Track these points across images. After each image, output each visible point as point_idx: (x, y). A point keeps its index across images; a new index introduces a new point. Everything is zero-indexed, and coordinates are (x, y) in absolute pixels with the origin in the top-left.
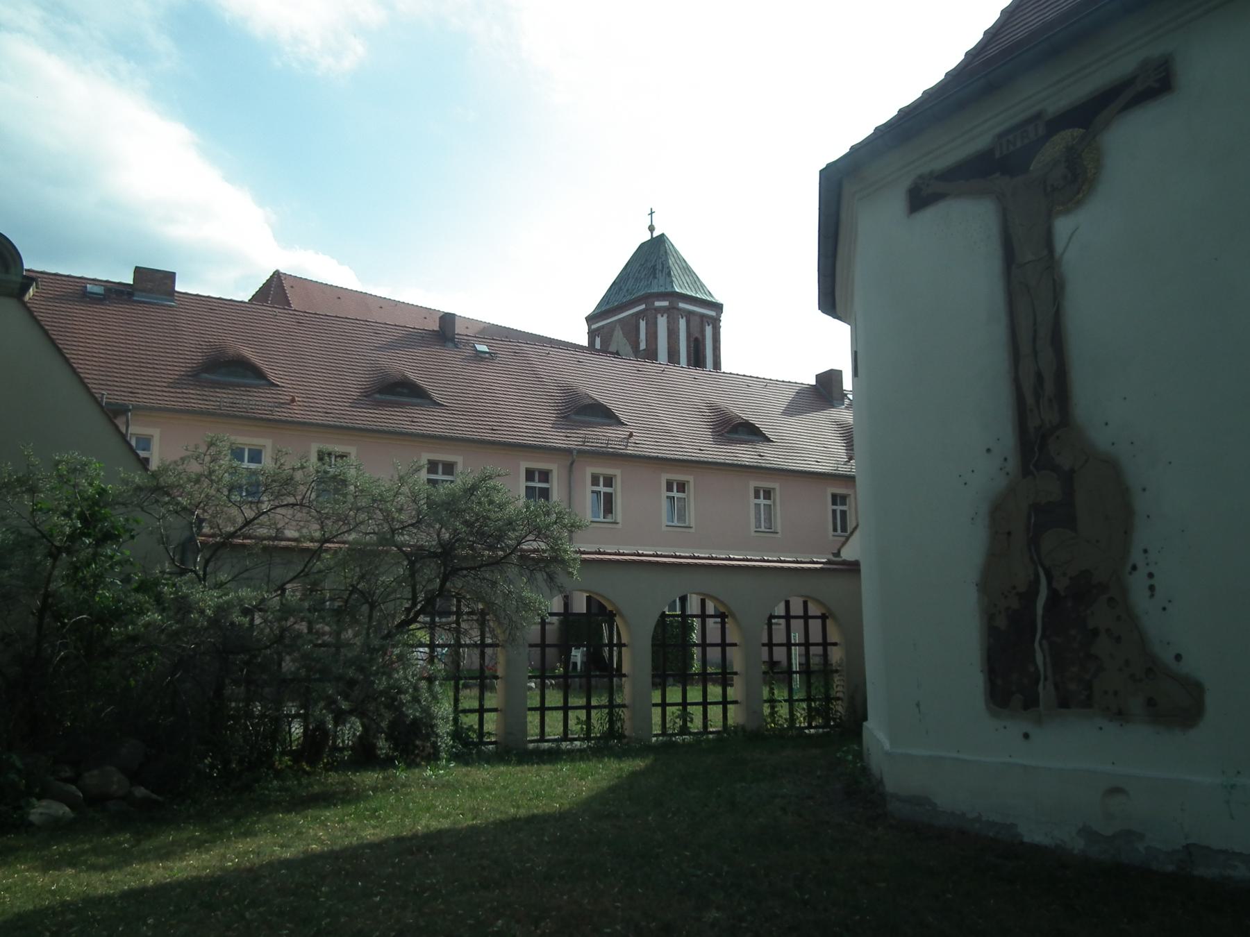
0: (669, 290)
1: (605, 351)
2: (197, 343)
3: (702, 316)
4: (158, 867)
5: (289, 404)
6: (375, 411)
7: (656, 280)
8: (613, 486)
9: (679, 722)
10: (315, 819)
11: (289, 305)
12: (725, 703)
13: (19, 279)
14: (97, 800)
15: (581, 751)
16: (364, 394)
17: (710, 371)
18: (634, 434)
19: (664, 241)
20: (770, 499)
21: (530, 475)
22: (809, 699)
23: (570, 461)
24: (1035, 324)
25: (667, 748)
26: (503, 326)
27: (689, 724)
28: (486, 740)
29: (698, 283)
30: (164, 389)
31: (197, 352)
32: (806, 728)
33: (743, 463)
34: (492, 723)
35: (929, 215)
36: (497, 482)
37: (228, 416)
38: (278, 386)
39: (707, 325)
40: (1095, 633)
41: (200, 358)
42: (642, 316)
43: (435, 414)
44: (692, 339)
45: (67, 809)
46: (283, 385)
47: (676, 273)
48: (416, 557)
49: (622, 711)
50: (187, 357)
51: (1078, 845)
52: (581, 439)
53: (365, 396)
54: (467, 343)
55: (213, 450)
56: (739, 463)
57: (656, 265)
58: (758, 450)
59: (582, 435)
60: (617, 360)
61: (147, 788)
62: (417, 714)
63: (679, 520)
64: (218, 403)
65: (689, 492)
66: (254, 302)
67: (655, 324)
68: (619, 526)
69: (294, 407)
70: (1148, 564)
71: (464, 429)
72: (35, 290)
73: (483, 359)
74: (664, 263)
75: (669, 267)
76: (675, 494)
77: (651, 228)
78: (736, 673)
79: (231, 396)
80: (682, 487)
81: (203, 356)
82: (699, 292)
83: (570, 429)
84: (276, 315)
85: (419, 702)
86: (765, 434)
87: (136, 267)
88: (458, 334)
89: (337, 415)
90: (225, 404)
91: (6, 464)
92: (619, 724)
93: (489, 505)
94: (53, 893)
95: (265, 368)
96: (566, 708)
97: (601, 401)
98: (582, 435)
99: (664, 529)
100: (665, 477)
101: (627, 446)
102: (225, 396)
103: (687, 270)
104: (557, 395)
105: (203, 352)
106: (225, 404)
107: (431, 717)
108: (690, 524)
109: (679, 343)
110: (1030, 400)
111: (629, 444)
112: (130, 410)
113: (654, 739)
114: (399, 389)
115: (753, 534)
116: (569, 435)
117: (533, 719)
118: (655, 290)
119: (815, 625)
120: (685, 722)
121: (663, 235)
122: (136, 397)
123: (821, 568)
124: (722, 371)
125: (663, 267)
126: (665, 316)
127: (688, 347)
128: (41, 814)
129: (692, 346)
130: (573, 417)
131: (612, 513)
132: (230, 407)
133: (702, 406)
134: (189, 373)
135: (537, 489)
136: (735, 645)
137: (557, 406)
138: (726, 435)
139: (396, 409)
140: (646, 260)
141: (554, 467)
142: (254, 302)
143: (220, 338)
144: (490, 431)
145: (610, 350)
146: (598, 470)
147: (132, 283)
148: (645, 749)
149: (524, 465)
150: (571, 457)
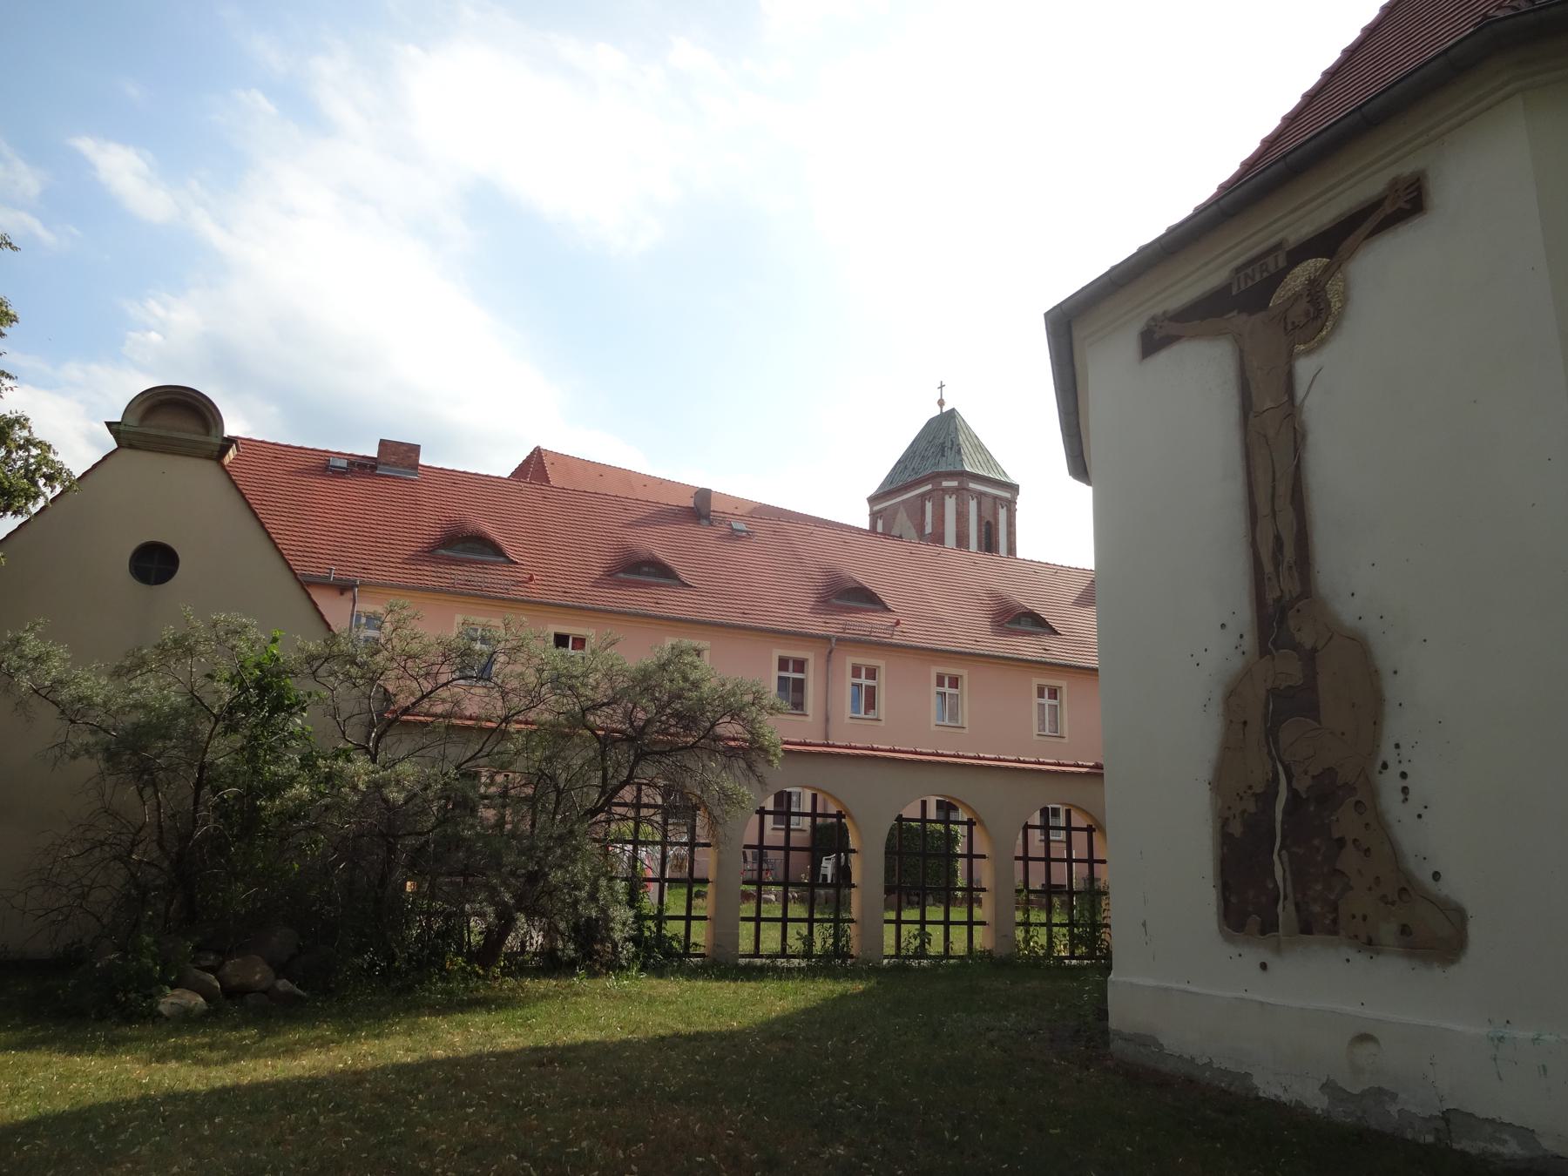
0: (959, 468)
1: (887, 534)
3: (996, 498)
4: (266, 1066)
7: (944, 458)
10: (459, 1025)
11: (548, 482)
12: (970, 923)
14: (234, 993)
15: (800, 970)
19: (954, 417)
20: (1056, 698)
21: (783, 664)
22: (1072, 924)
23: (828, 650)
24: (1274, 480)
25: (901, 968)
26: (648, 474)
28: (692, 951)
29: (992, 463)
31: (436, 527)
32: (1066, 958)
33: (1025, 657)
34: (700, 934)
35: (1163, 358)
37: (462, 594)
38: (516, 563)
40: (1341, 842)
43: (682, 595)
44: (983, 523)
45: (201, 999)
46: (522, 562)
47: (966, 451)
48: (607, 742)
50: (425, 532)
51: (1318, 1102)
53: (609, 576)
54: (723, 520)
56: (1021, 656)
57: (944, 443)
61: (292, 982)
63: (950, 719)
64: (453, 581)
67: (943, 505)
68: (882, 724)
70: (1400, 762)
72: (236, 453)
73: (739, 538)
74: (954, 440)
75: (958, 445)
76: (946, 689)
77: (941, 403)
78: (984, 890)
79: (466, 573)
80: (954, 683)
85: (597, 900)
86: (1051, 626)
88: (714, 511)
89: (577, 596)
94: (140, 1086)
95: (504, 544)
96: (785, 920)
97: (867, 585)
99: (934, 728)
100: (935, 670)
101: (892, 635)
102: (460, 573)
103: (980, 448)
105: (442, 528)
107: (608, 919)
108: (962, 723)
109: (968, 527)
110: (1268, 568)
111: (895, 633)
112: (357, 586)
113: (886, 961)
114: (646, 569)
115: (1036, 738)
116: (828, 621)
119: (1080, 839)
120: (923, 944)
121: (953, 410)
122: (368, 573)
123: (1087, 773)
125: (952, 445)
126: (954, 497)
127: (979, 531)
128: (172, 1004)
131: (874, 709)
134: (426, 550)
136: (984, 857)
137: (817, 590)
139: (641, 590)
140: (934, 437)
144: (740, 615)
145: (892, 534)
146: (859, 661)
148: (875, 970)
149: (777, 653)
150: (829, 645)
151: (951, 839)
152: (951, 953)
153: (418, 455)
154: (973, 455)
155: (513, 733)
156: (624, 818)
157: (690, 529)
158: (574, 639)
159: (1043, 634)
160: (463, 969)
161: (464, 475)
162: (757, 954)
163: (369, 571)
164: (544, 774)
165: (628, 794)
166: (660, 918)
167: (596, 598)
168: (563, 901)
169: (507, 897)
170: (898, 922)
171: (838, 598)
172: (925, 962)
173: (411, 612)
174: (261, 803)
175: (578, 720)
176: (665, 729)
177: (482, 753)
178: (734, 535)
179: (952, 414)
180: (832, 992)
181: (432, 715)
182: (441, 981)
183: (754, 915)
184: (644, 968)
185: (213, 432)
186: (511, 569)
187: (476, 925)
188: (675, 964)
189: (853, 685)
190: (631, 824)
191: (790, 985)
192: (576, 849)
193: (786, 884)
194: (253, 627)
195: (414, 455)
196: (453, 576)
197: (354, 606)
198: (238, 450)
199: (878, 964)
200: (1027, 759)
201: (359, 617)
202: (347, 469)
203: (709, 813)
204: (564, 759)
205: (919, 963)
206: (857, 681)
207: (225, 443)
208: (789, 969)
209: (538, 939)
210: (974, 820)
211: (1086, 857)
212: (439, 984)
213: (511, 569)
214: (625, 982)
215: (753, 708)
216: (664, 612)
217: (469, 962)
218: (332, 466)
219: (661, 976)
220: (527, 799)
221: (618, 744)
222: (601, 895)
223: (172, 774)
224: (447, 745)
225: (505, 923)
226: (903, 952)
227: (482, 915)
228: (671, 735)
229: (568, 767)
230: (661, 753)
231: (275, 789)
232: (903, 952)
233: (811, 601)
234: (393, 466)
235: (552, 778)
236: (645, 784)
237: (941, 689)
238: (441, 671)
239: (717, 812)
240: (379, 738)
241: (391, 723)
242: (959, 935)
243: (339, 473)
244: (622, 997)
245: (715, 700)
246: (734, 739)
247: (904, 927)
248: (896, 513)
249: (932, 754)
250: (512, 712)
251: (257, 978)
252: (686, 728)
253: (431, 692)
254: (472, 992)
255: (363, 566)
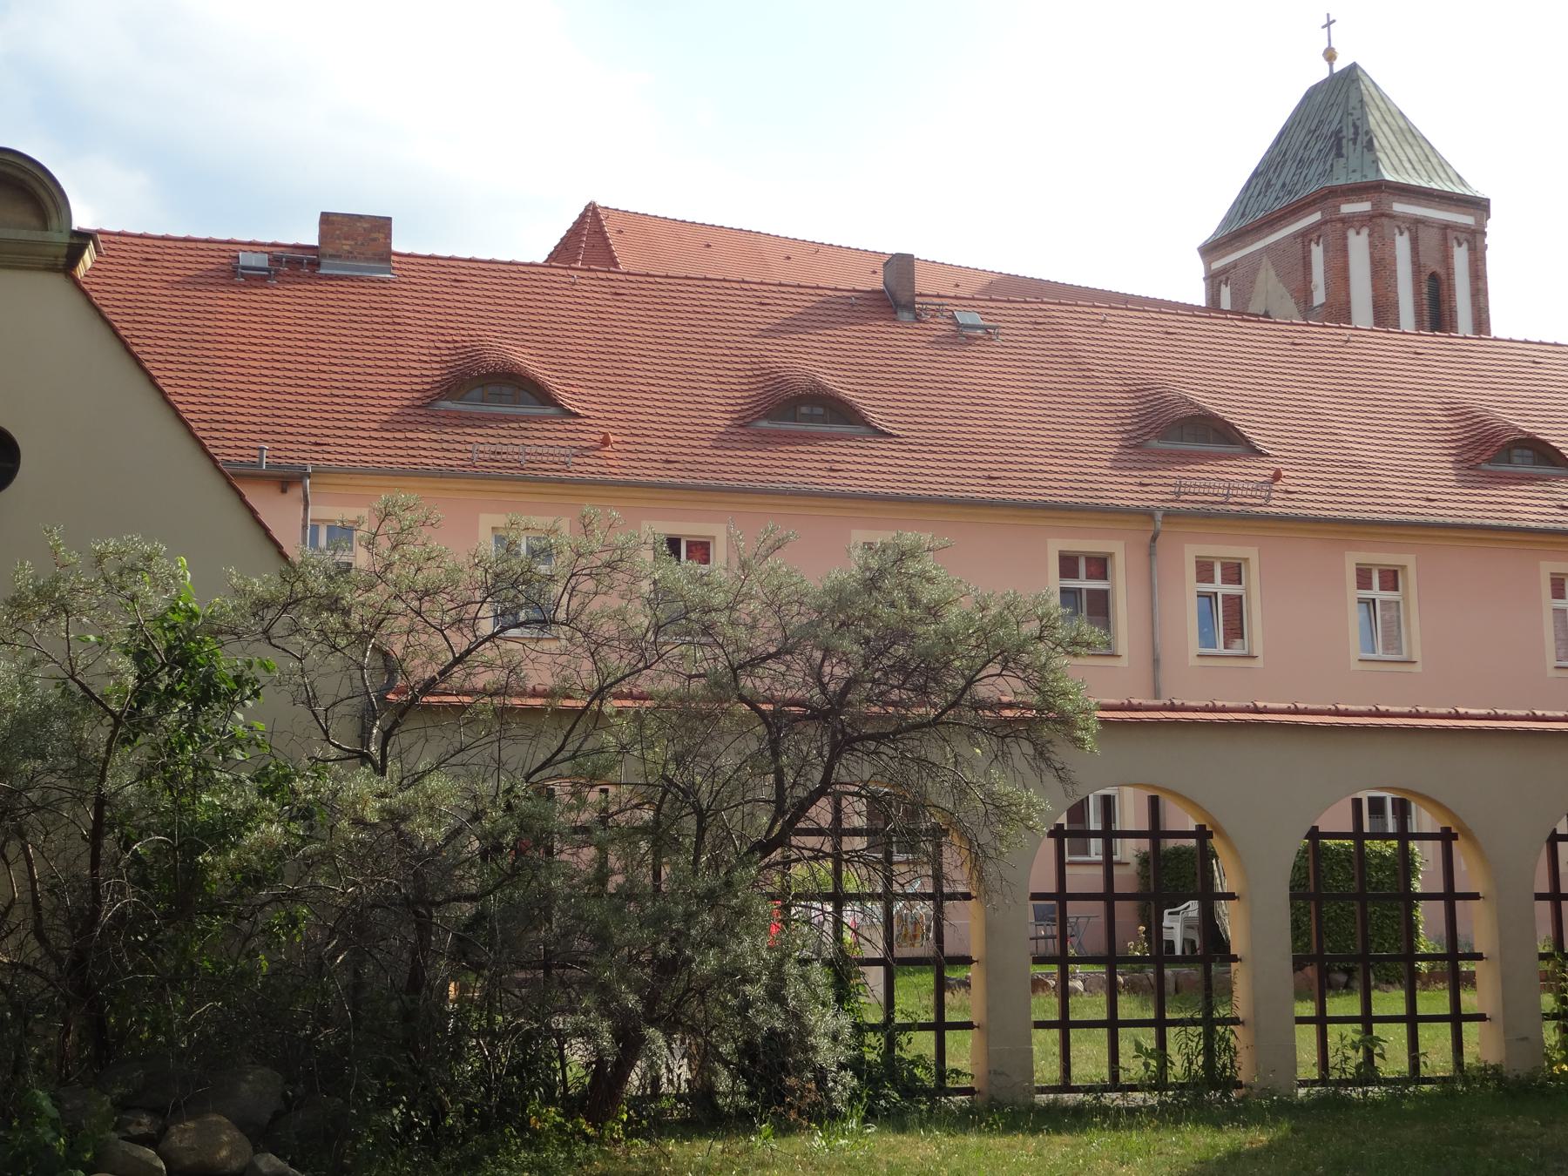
0: (1371, 177)
1: (1240, 312)
2: (432, 344)
3: (1446, 227)
5: (598, 449)
6: (760, 454)
7: (1342, 161)
8: (1243, 582)
9: (1359, 1057)
11: (616, 265)
12: (1456, 1018)
13: (66, 239)
16: (741, 422)
17: (1466, 338)
18: (1284, 473)
20: (1396, 588)
21: (1068, 565)
27: (1377, 1061)
30: (374, 434)
33: (1524, 524)
34: (963, 1053)
36: (929, 563)
37: (487, 477)
38: (577, 415)
39: (1455, 244)
41: (438, 372)
42: (1315, 236)
44: (1424, 277)
47: (1384, 142)
49: (1233, 1032)
52: (1173, 489)
53: (741, 426)
55: (390, 526)
56: (1515, 523)
57: (1340, 131)
58: (1556, 496)
59: (1173, 481)
60: (1248, 324)
62: (778, 1024)
63: (1386, 648)
64: (470, 455)
65: (1406, 587)
66: (553, 264)
67: (1344, 250)
69: (608, 455)
71: (933, 480)
74: (1358, 123)
75: (1367, 133)
76: (1376, 593)
77: (1330, 55)
79: (492, 440)
80: (1391, 579)
81: (442, 369)
82: (1437, 179)
83: (1150, 469)
84: (574, 284)
85: (782, 1001)
87: (323, 214)
88: (921, 295)
89: (688, 466)
90: (481, 455)
91: (22, 564)
92: (1225, 1059)
93: (911, 608)
96: (1113, 1024)
97: (1214, 409)
98: (1173, 481)
100: (1353, 559)
101: (1269, 498)
102: (480, 439)
103: (1409, 134)
104: (1122, 401)
106: (481, 455)
107: (805, 1031)
111: (1274, 495)
112: (309, 476)
113: (1302, 1092)
114: (804, 410)
115: (1551, 673)
116: (1146, 481)
117: (1045, 1043)
118: (1342, 181)
121: (1354, 67)
124: (1492, 337)
125: (1356, 133)
126: (1365, 232)
127: (1417, 292)
129: (1425, 290)
130: (1155, 444)
131: (1242, 637)
132: (492, 460)
133: (1433, 409)
134: (419, 403)
135: (1084, 594)
136: (1475, 896)
138: (1485, 466)
141: (1118, 548)
142: (553, 264)
143: (463, 332)
145: (1250, 310)
147: (315, 242)
148: (1286, 1108)
149: (1056, 545)
151: (1405, 865)
152: (1424, 1072)
153: (388, 236)
154: (1398, 150)
155: (611, 716)
156: (818, 855)
157: (880, 329)
158: (689, 544)
159: (1558, 478)
160: (559, 1128)
161: (471, 265)
162: (1066, 1087)
163: (325, 448)
164: (670, 782)
165: (821, 813)
166: (890, 1030)
167: (722, 468)
168: (724, 1006)
169: (632, 1000)
170: (1322, 1021)
171: (1163, 436)
172: (1375, 1091)
173: (418, 515)
174: (204, 858)
175: (726, 686)
176: (882, 693)
177: (565, 754)
178: (961, 336)
179: (1352, 75)
180: (1214, 1148)
181: (466, 694)
182: (525, 1148)
183: (1104, 1016)
184: (871, 1115)
185: (54, 223)
186: (568, 427)
187: (577, 1055)
188: (923, 1107)
189: (1200, 595)
190: (829, 865)
191: (1135, 1138)
192: (740, 912)
193: (1111, 959)
194: (161, 557)
195: (382, 235)
196: (469, 447)
197: (306, 510)
198: (98, 252)
199: (1289, 1096)
200: (1549, 714)
201: (315, 529)
202: (268, 270)
203: (970, 841)
204: (707, 756)
205: (1365, 1093)
206: (1207, 588)
207: (75, 241)
208: (1131, 1112)
209: (683, 1071)
210: (1454, 831)
211: (1440, 889)
212: (523, 1154)
213: (568, 427)
214: (842, 1142)
215: (1041, 646)
216: (942, 490)
217: (569, 1114)
218: (244, 268)
219: (902, 1129)
220: (644, 830)
221: (800, 726)
222: (789, 992)
223: (49, 817)
224: (503, 742)
225: (630, 1044)
226: (1335, 1075)
227: (587, 1034)
228: (894, 704)
229: (714, 772)
230: (879, 738)
231: (223, 831)
232: (1335, 1075)
233: (1112, 447)
234: (347, 258)
235: (690, 791)
236: (852, 794)
237: (1366, 594)
238: (479, 615)
239: (984, 837)
240: (387, 736)
241: (403, 711)
242: (1436, 1043)
243: (256, 279)
244: (839, 1167)
245: (970, 636)
246: (1010, 706)
247: (1332, 1029)
248: (1255, 271)
249: (1369, 714)
250: (609, 681)
251: (224, 1153)
252: (922, 690)
253: (469, 652)
254: (580, 1165)
255: (313, 439)
